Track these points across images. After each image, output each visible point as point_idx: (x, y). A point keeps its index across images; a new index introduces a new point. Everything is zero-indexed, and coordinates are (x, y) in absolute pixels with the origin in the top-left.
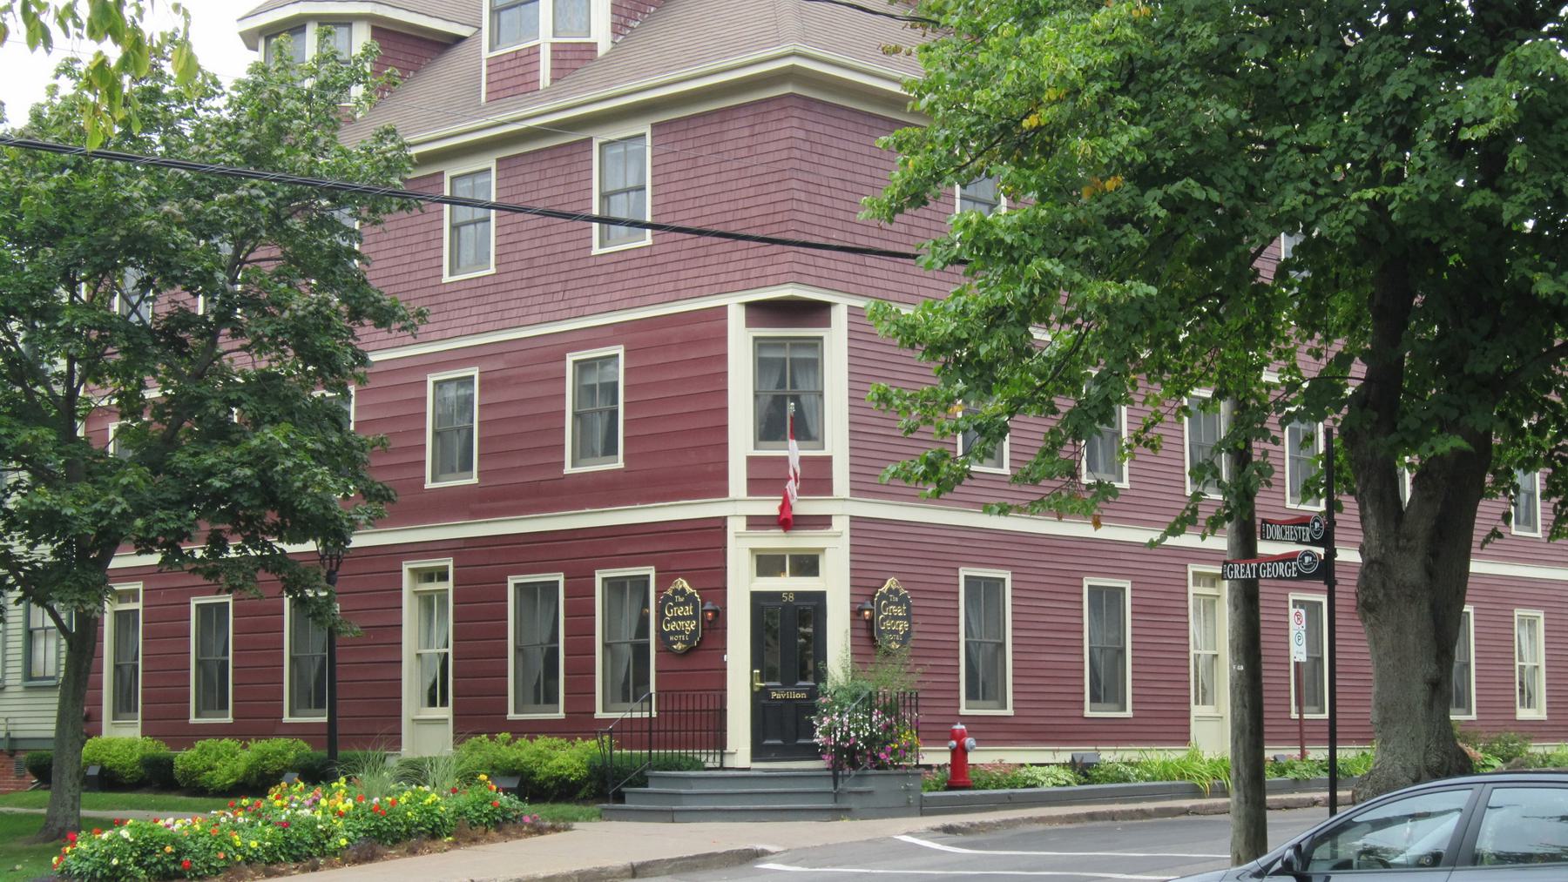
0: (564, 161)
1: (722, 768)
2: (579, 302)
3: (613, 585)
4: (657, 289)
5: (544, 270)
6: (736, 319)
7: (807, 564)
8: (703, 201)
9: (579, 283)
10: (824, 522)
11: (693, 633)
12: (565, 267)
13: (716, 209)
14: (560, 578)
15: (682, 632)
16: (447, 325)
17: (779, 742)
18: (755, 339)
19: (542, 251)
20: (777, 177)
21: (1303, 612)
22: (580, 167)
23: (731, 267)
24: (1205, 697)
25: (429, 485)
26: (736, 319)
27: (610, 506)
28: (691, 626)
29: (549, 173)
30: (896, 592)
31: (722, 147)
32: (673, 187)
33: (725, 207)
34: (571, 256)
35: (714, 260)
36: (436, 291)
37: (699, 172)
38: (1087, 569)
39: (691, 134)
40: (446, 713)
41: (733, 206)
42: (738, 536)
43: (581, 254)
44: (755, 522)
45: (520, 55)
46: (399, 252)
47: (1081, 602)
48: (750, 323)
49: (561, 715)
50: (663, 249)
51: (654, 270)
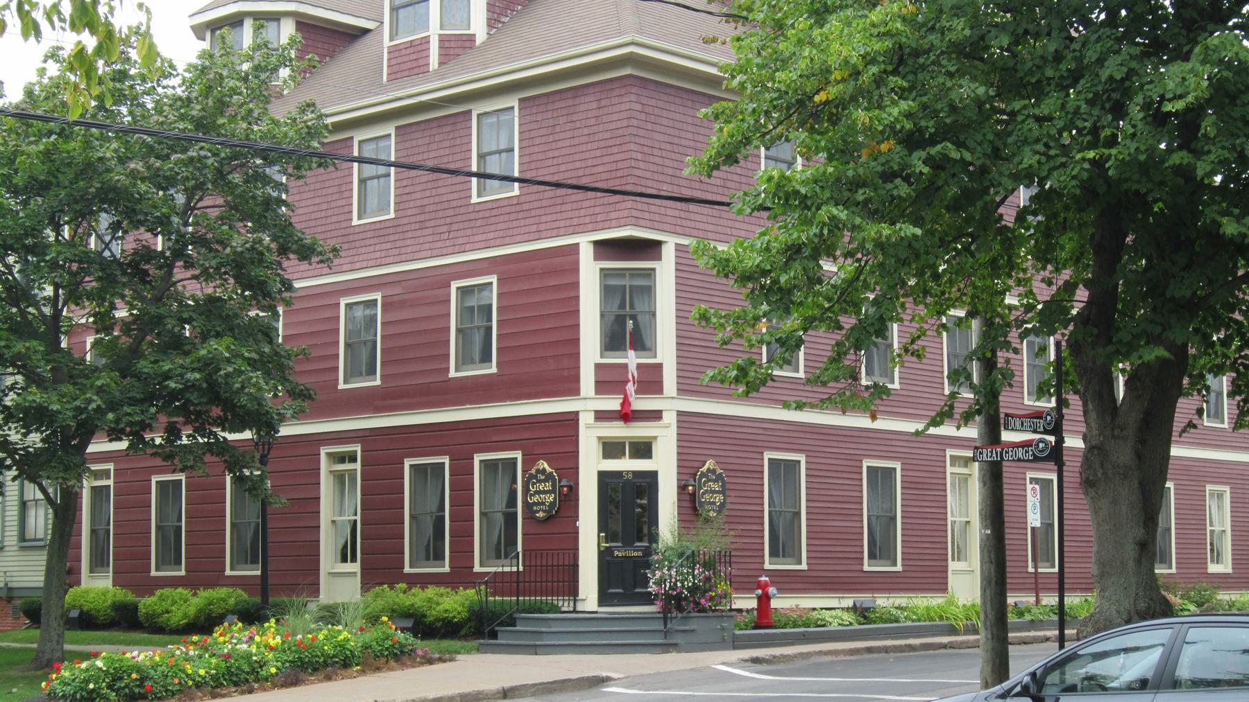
0: (449, 128)
1: (575, 611)
2: (461, 241)
3: (488, 466)
4: (523, 230)
5: (433, 215)
6: (586, 254)
7: (643, 449)
9: (461, 226)
10: (656, 415)
11: (552, 504)
12: (450, 212)
13: (570, 166)
14: (446, 460)
15: (543, 503)
16: (356, 258)
17: (621, 591)
18: (602, 270)
19: (432, 200)
20: (618, 141)
21: (1037, 487)
22: (462, 133)
23: (583, 212)
24: (960, 555)
25: (341, 386)
26: (586, 254)
27: (486, 402)
28: (550, 498)
30: (714, 471)
31: (575, 117)
32: (536, 149)
33: (578, 165)
34: (454, 204)
35: (568, 207)
36: (347, 232)
37: (557, 137)
39: (550, 107)
40: (355, 567)
41: (583, 164)
42: (588, 427)
44: (601, 416)
45: (414, 44)
46: (317, 201)
47: (861, 480)
48: (597, 257)
49: (447, 569)
51: (521, 215)
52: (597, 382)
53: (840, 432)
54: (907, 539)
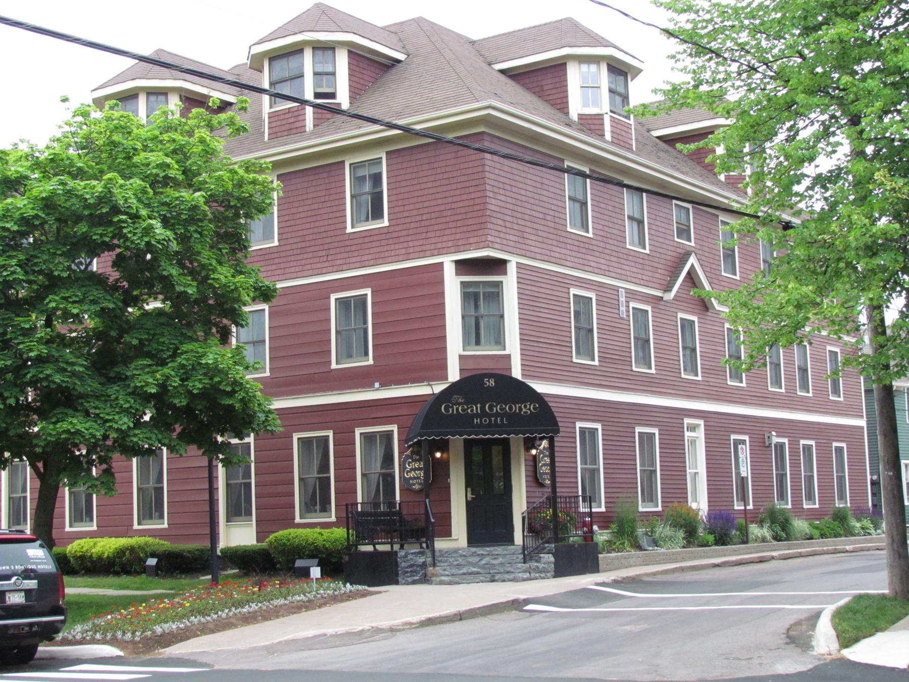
0: (325, 175)
2: (338, 262)
5: (312, 243)
6: (449, 270)
8: (424, 199)
13: (432, 203)
14: (330, 434)
18: (462, 283)
23: (445, 238)
26: (449, 270)
27: (401, 384)
29: (314, 183)
31: (436, 165)
32: (403, 190)
33: (440, 202)
38: (637, 422)
41: (445, 201)
43: (339, 232)
45: (291, 110)
48: (458, 273)
50: (397, 228)
52: (460, 370)
53: (623, 407)
54: (664, 486)
